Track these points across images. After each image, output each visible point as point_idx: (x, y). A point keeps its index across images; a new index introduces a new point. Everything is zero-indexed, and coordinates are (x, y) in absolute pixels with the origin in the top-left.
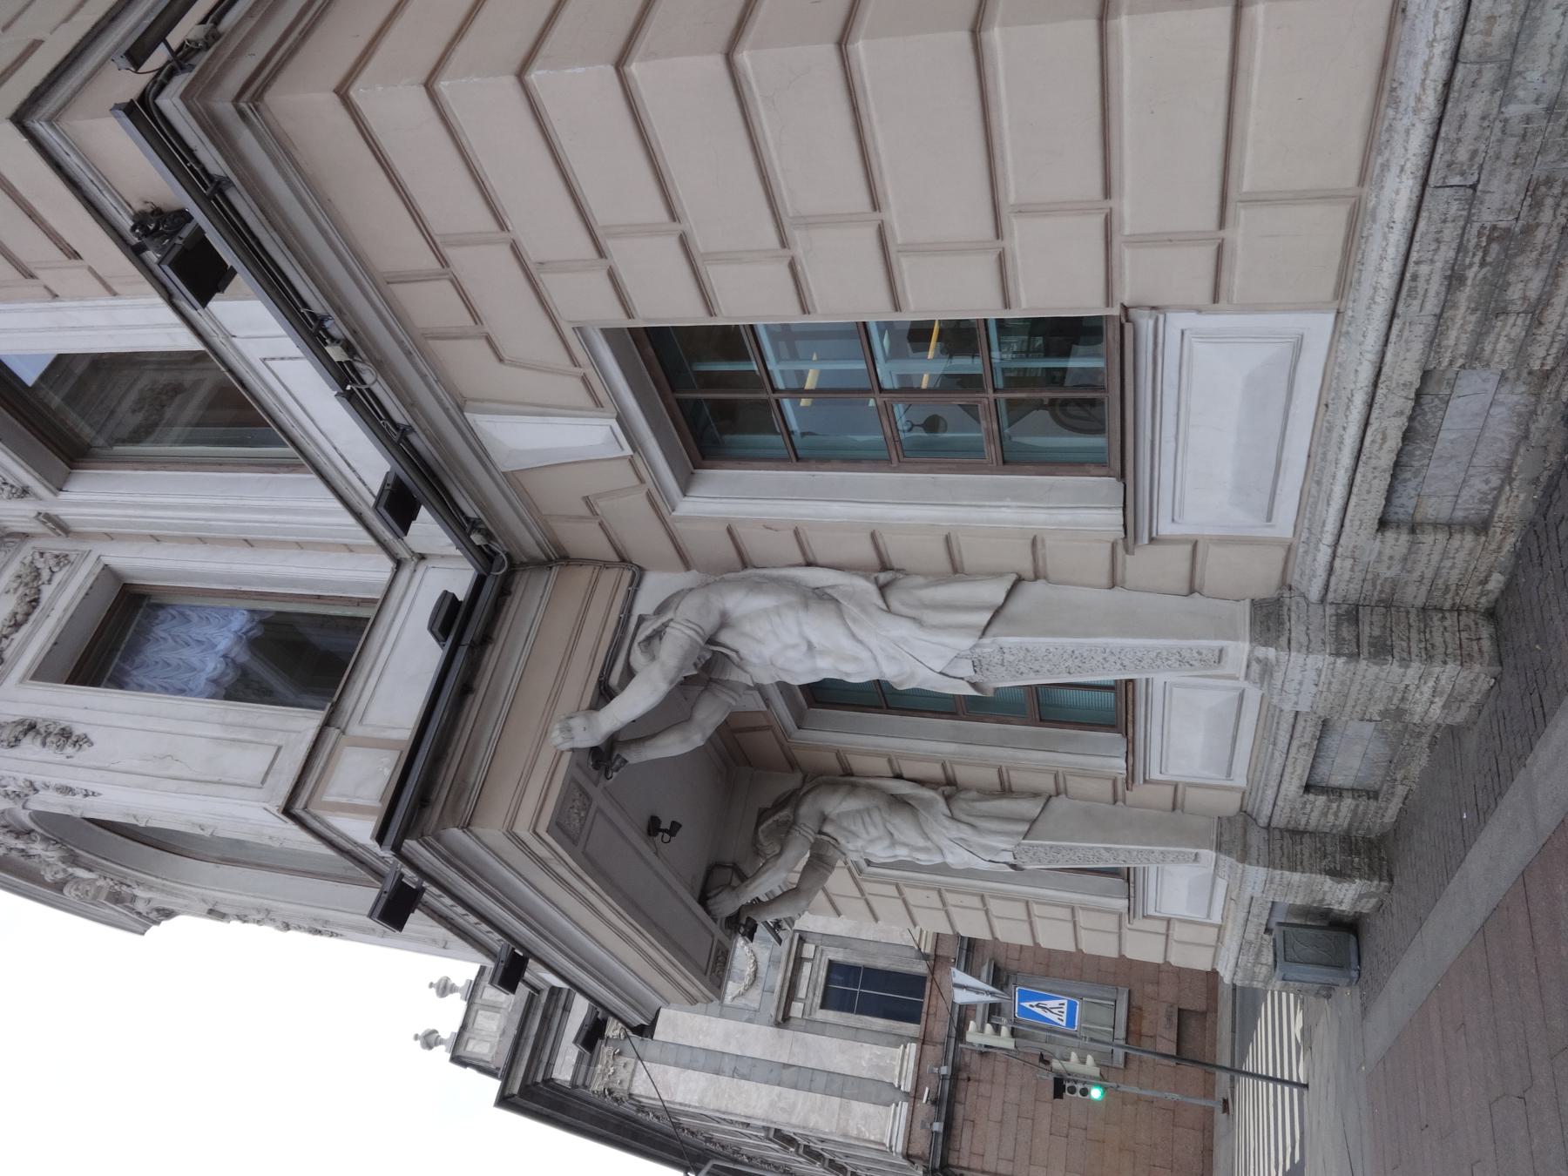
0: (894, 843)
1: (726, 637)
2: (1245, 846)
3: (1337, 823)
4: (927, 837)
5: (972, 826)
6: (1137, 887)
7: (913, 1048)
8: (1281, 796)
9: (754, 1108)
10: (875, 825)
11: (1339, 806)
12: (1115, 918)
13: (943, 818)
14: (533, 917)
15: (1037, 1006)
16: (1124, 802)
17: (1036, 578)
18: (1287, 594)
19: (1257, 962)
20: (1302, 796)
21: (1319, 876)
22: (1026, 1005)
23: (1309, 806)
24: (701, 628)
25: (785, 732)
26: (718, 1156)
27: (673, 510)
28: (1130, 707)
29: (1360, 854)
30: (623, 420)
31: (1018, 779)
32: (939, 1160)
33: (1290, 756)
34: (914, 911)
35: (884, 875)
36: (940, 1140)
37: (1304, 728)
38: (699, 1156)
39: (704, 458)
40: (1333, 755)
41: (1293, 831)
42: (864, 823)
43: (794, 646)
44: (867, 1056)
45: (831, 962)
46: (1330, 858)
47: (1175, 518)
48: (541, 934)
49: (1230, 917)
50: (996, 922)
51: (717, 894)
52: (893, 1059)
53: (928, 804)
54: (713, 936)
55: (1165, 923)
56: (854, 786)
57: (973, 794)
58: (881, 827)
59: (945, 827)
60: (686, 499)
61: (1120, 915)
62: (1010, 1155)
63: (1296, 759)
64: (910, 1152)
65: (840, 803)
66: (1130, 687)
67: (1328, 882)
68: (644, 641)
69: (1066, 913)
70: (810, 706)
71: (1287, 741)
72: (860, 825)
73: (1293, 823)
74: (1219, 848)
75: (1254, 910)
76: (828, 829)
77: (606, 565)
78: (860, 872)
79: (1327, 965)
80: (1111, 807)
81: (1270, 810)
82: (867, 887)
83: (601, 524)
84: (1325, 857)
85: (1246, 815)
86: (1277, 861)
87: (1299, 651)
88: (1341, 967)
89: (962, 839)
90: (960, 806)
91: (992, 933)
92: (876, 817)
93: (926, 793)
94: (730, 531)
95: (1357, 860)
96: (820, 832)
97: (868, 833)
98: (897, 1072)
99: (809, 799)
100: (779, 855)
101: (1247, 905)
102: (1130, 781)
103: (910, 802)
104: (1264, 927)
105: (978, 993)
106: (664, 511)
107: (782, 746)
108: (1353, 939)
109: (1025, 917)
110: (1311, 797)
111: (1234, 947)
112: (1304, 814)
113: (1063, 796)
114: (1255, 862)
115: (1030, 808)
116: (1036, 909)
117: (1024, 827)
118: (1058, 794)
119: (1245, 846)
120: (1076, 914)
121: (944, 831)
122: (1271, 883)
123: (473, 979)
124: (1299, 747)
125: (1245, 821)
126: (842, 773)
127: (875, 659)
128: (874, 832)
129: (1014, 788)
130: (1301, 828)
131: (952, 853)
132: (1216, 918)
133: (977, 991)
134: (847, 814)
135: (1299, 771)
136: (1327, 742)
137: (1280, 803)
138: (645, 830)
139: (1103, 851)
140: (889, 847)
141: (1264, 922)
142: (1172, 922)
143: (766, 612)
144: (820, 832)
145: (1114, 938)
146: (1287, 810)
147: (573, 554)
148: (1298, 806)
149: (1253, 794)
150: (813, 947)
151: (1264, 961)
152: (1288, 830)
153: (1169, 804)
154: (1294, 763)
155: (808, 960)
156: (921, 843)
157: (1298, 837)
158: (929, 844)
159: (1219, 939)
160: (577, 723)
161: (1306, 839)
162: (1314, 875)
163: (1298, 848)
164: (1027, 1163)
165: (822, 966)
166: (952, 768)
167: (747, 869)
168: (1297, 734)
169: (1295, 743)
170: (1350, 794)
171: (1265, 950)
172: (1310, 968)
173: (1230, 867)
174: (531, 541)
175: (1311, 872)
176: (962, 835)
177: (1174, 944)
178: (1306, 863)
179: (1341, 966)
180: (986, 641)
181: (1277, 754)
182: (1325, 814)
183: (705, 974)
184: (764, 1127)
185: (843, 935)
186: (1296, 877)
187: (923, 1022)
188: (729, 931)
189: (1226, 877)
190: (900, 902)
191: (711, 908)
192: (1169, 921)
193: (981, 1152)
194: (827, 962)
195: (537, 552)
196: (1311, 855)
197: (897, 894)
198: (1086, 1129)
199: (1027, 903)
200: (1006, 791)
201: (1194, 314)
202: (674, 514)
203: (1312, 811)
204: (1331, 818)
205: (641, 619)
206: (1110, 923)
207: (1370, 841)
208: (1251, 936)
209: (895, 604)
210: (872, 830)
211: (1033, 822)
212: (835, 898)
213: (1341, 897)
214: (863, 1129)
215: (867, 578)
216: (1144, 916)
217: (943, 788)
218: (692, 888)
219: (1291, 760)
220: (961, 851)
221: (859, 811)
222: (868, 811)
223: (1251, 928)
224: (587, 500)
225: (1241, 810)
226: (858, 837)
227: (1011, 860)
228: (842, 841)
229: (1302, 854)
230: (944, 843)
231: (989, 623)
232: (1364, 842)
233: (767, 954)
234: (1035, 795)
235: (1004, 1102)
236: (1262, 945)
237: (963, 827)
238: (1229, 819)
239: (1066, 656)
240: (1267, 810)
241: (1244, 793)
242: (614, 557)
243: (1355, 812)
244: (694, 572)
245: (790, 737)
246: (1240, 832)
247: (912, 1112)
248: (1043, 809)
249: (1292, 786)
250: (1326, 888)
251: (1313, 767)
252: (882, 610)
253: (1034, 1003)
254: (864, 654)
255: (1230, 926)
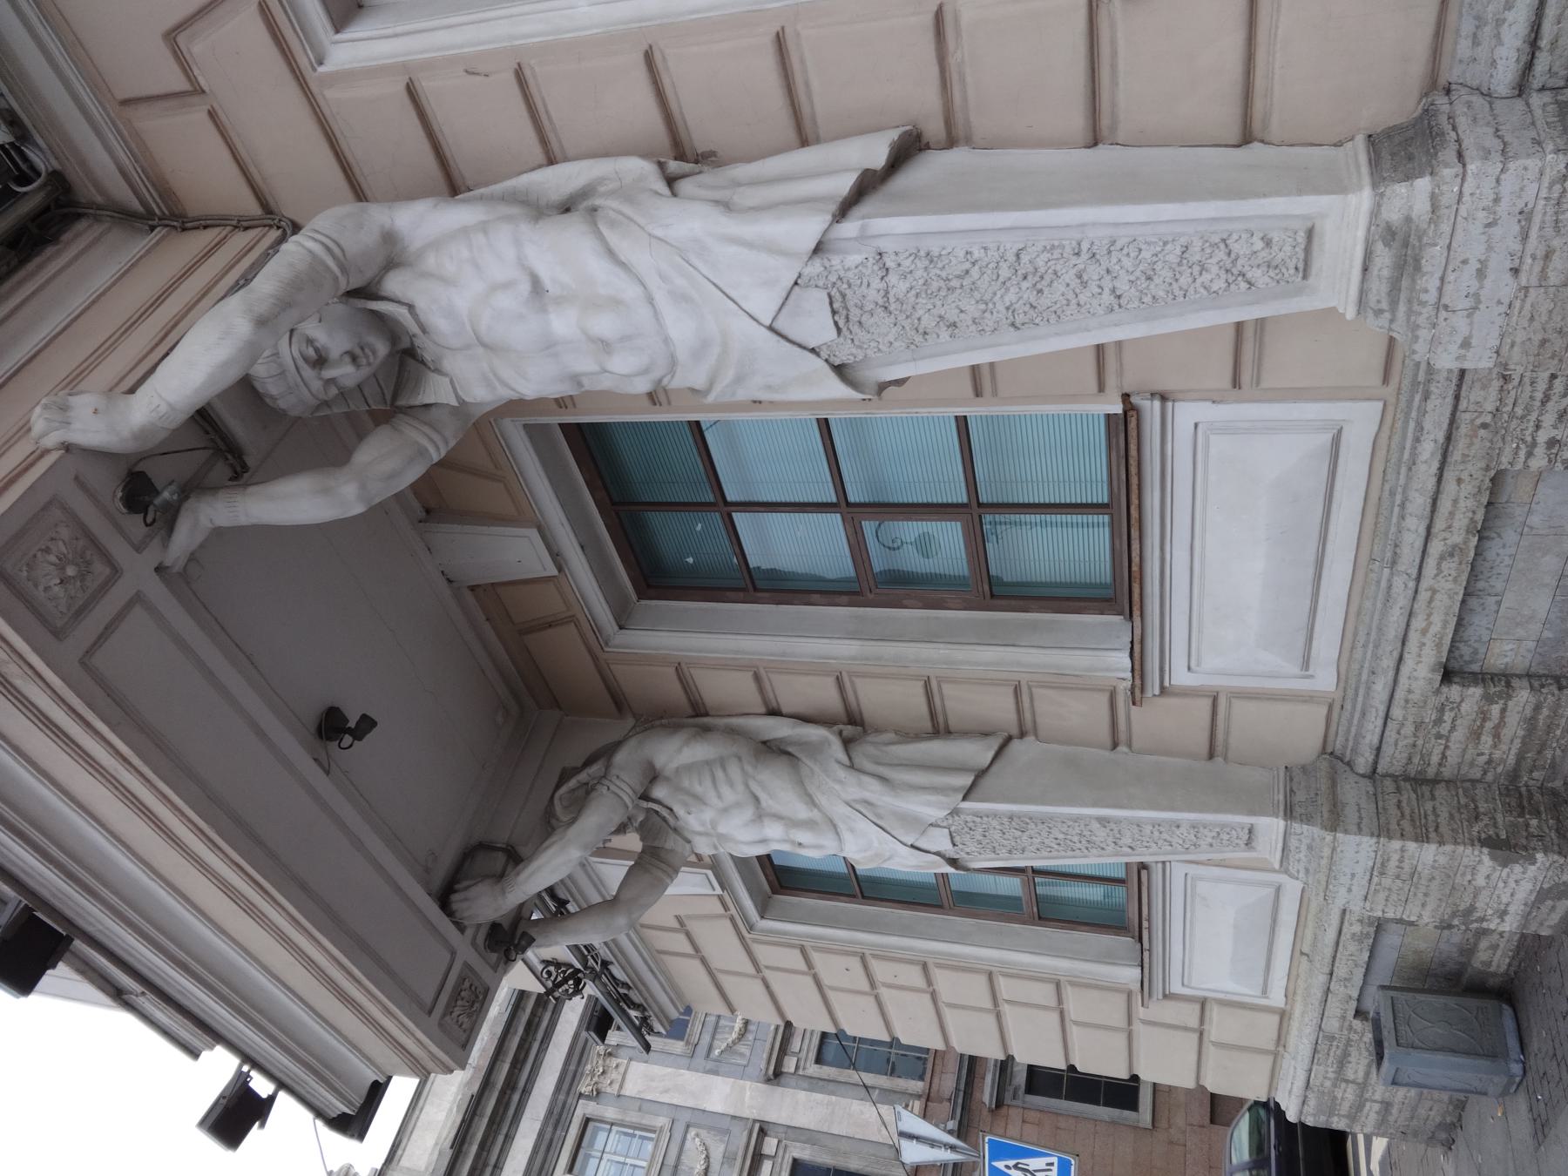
0: (760, 815)
1: (394, 284)
2: (1335, 805)
3: (1497, 755)
4: (812, 802)
5: (883, 779)
6: (1154, 936)
8: (1400, 694)
10: (731, 784)
11: (1503, 711)
12: (1121, 1000)
13: (837, 766)
14: (44, 834)
15: (1016, 1167)
16: (1130, 746)
17: (951, 142)
18: (1441, 101)
19: (1340, 1078)
20: (1437, 692)
21: (1469, 850)
22: (1000, 1165)
23: (1448, 716)
24: (339, 245)
25: (597, 630)
27: (321, 63)
28: (1134, 480)
29: (1539, 813)
31: (960, 703)
33: (1424, 584)
34: (831, 995)
35: (785, 933)
37: (1455, 502)
40: (1499, 585)
41: (1414, 779)
43: (507, 286)
45: (795, 1161)
46: (1486, 820)
47: (1193, 665)
48: (71, 876)
49: (1299, 992)
50: (949, 1015)
51: (469, 887)
53: (814, 749)
54: (453, 953)
55: (1197, 1007)
56: (706, 729)
58: (741, 788)
59: (840, 782)
61: (1130, 994)
63: (1434, 591)
65: (680, 750)
66: (1144, 873)
67: (1485, 862)
69: (1044, 993)
70: (640, 598)
71: (1419, 543)
72: (708, 782)
73: (1416, 760)
74: (1289, 813)
75: (1341, 971)
76: (659, 792)
77: (242, 224)
78: (751, 928)
79: (1467, 1053)
80: (1107, 754)
81: (1378, 731)
82: (763, 953)
83: (212, 114)
84: (1477, 818)
85: (1334, 758)
86: (1394, 826)
88: (1493, 1056)
89: (867, 803)
90: (863, 753)
92: (734, 770)
93: (815, 733)
94: (411, 91)
95: (1534, 822)
96: (645, 797)
97: (719, 797)
100: (573, 821)
101: (1328, 959)
102: (1137, 692)
103: (790, 749)
104: (1354, 1004)
105: (933, 1146)
106: (303, 62)
107: (595, 659)
108: (1507, 1011)
109: (988, 1004)
110: (1454, 691)
111: (1305, 1049)
112: (1439, 736)
113: (1030, 739)
114: (1355, 828)
116: (1005, 987)
118: (1022, 735)
119: (1335, 805)
120: (1063, 991)
121: (837, 787)
122: (1382, 874)
123: (379, 1167)
124: (1442, 558)
125: (1333, 767)
126: (690, 711)
127: (650, 300)
128: (729, 795)
129: (952, 729)
130: (1431, 772)
131: (852, 830)
132: (1277, 998)
133: (932, 1143)
134: (689, 768)
135: (1436, 628)
136: (1494, 550)
137: (1397, 712)
138: (313, 729)
139: (1095, 825)
140: (753, 821)
141: (1355, 994)
142: (1208, 1007)
143: (464, 232)
144: (645, 797)
145: (1120, 1041)
146: (1409, 729)
147: (194, 208)
148: (1430, 715)
149: (1348, 706)
150: (776, 1141)
151: (1351, 1076)
152: (1407, 778)
153: (1204, 750)
154: (1431, 601)
155: (768, 1157)
156: (802, 812)
157: (1426, 789)
158: (815, 814)
159: (1281, 1039)
161: (1441, 791)
162: (1461, 848)
163: (1429, 806)
165: (784, 1167)
166: (852, 683)
167: (523, 851)
168: (1439, 524)
169: (1436, 548)
170: (1525, 683)
171: (1353, 1051)
172: (1439, 1057)
173: (1310, 848)
174: (113, 167)
175: (1456, 843)
176: (867, 795)
177: (1212, 1048)
178: (1444, 829)
179: (1494, 1054)
180: (849, 228)
181: (1398, 582)
182: (1476, 735)
183: (430, 1013)
185: (812, 1127)
186: (1428, 855)
188: (494, 957)
189: (1302, 875)
190: (809, 980)
191: (455, 907)
192: (1203, 1003)
194: (791, 1160)
195: (122, 193)
196: (1452, 816)
197: (802, 966)
199: (990, 975)
201: (1209, 404)
202: (321, 69)
203: (1453, 728)
204: (1487, 740)
206: (1112, 1009)
207: (1554, 793)
208: (1332, 1025)
209: (860, 760)
210: (725, 790)
211: (981, 774)
212: (722, 978)
213: (1505, 899)
216: (1165, 996)
217: (841, 727)
218: (427, 870)
219: (1424, 596)
220: (863, 825)
221: (708, 763)
222: (722, 762)
223: (1334, 1008)
224: (678, 918)
225: (1324, 751)
226: (705, 804)
227: (945, 845)
228: (680, 811)
229: (1437, 816)
230: (840, 811)
232: (1542, 794)
233: (722, 1148)
236: (1349, 1040)
237: (866, 779)
238: (1304, 769)
239: (1005, 272)
240: (1371, 738)
241: (1331, 707)
242: (253, 208)
243: (1531, 723)
245: (607, 644)
246: (1324, 784)
249: (1421, 669)
250: (1480, 881)
251: (1460, 624)
253: (1011, 1163)
254: (631, 291)
255: (1298, 1010)
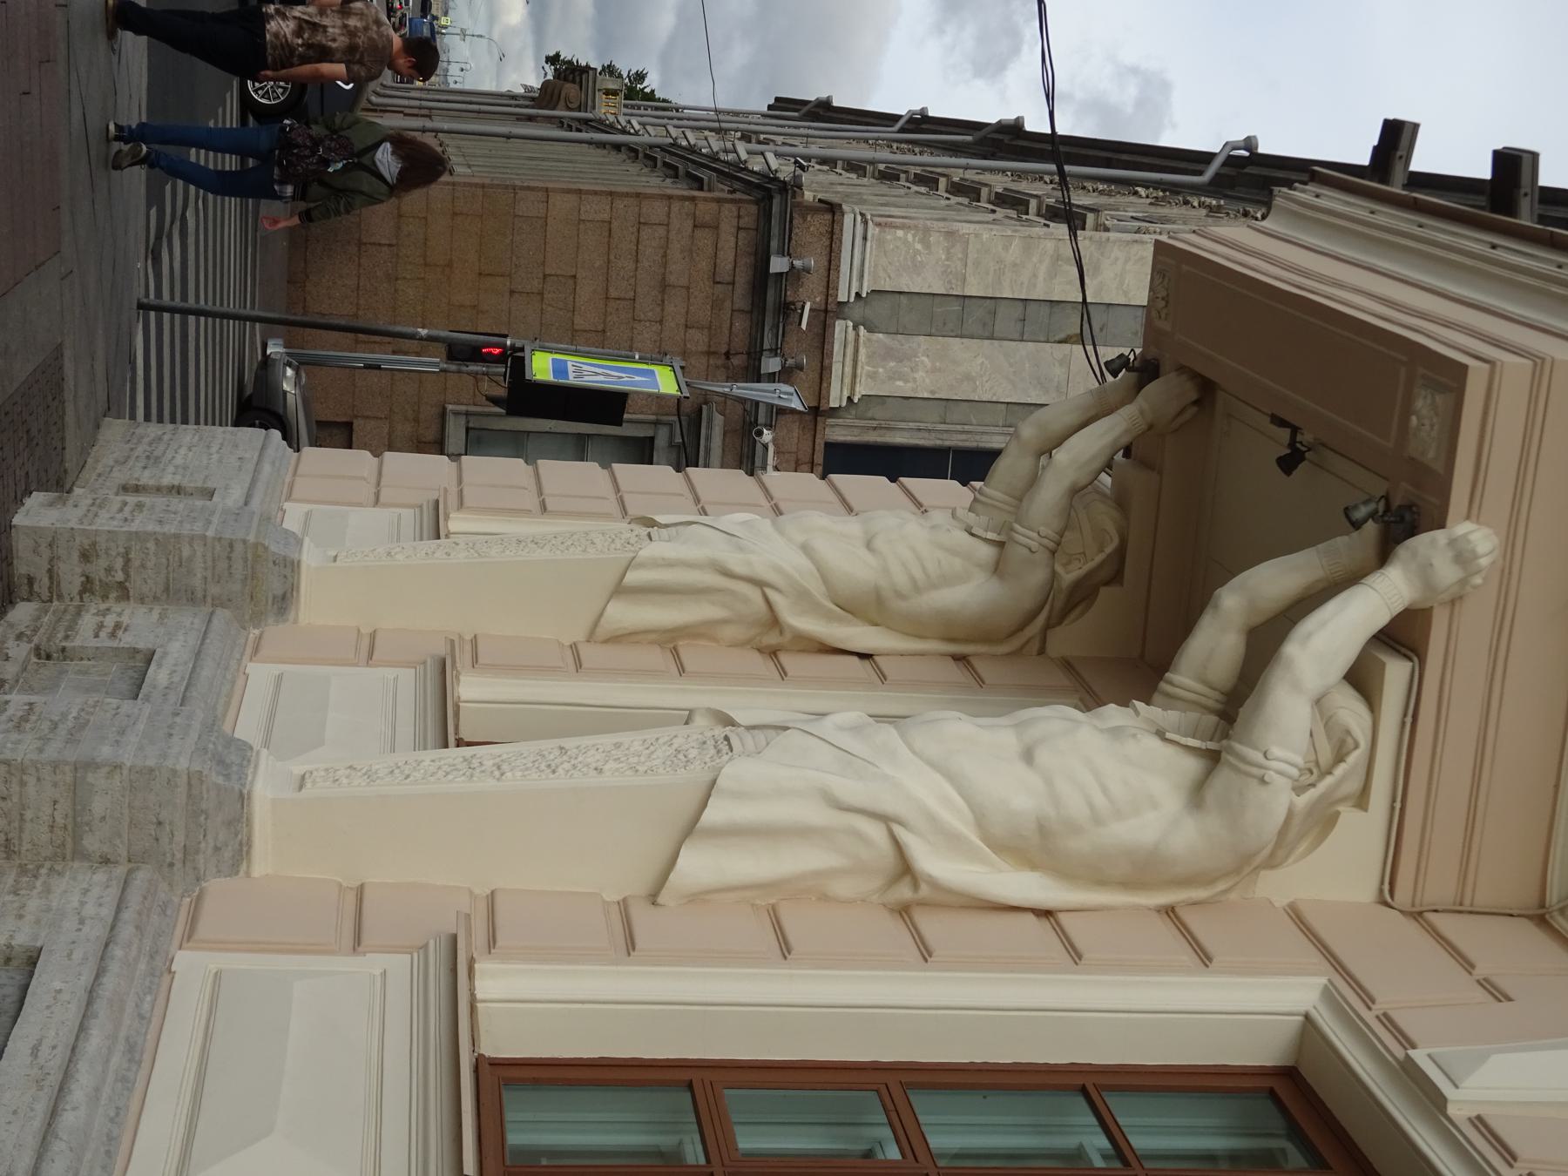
5: (728, 574)
7: (836, 398)
9: (1127, 261)
26: (1197, 190)
30: (1432, 1101)
32: (776, 209)
36: (774, 244)
38: (1232, 187)
39: (1289, 1074)
42: (924, 569)
44: (920, 375)
52: (872, 376)
57: (729, 632)
60: (1302, 1009)
62: (646, 233)
64: (828, 217)
68: (1348, 753)
87: (174, 772)
91: (688, 479)
92: (901, 580)
98: (862, 351)
99: (1028, 603)
115: (624, 615)
117: (632, 577)
134: (946, 580)
144: (1001, 545)
160: (1447, 573)
164: (615, 224)
184: (1107, 229)
187: (820, 447)
193: (698, 233)
198: (512, 292)
200: (671, 641)
205: (1361, 800)
211: (690, 829)
214: (919, 246)
215: (935, 884)
221: (934, 586)
222: (917, 588)
231: (704, 805)
234: (618, 638)
235: (661, 322)
244: (1281, 901)
247: (830, 286)
248: (601, 615)
252: (900, 823)
